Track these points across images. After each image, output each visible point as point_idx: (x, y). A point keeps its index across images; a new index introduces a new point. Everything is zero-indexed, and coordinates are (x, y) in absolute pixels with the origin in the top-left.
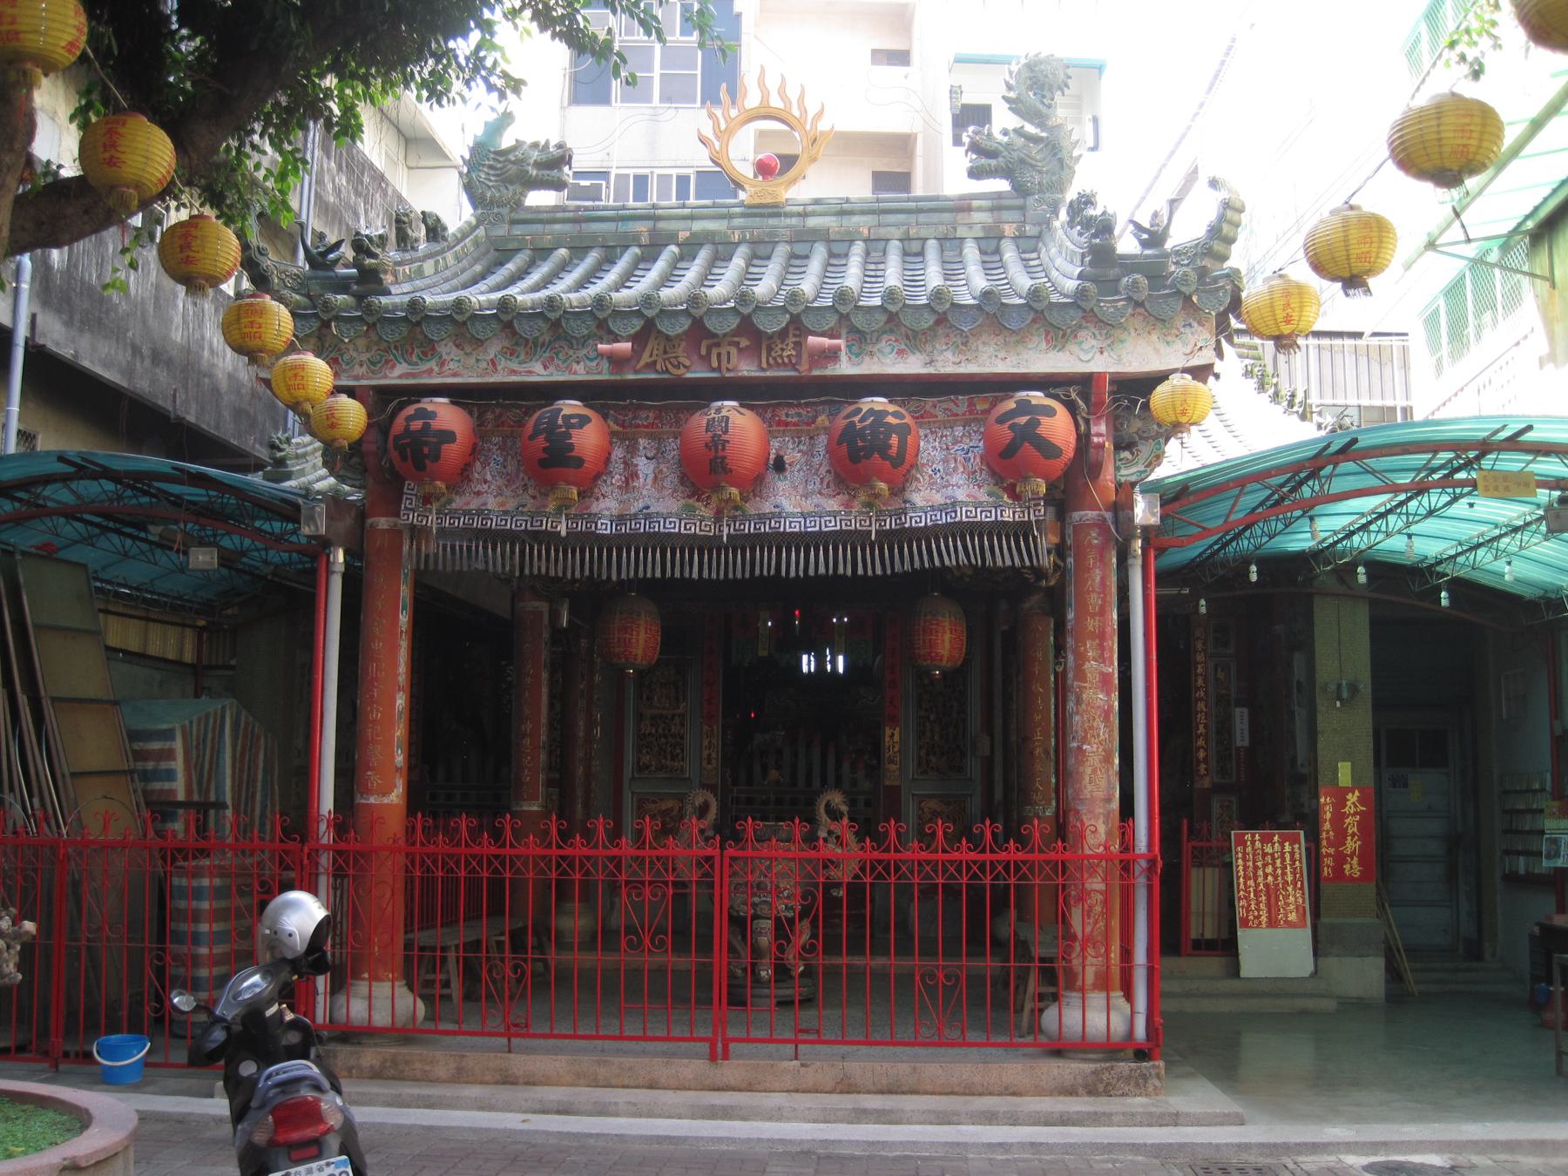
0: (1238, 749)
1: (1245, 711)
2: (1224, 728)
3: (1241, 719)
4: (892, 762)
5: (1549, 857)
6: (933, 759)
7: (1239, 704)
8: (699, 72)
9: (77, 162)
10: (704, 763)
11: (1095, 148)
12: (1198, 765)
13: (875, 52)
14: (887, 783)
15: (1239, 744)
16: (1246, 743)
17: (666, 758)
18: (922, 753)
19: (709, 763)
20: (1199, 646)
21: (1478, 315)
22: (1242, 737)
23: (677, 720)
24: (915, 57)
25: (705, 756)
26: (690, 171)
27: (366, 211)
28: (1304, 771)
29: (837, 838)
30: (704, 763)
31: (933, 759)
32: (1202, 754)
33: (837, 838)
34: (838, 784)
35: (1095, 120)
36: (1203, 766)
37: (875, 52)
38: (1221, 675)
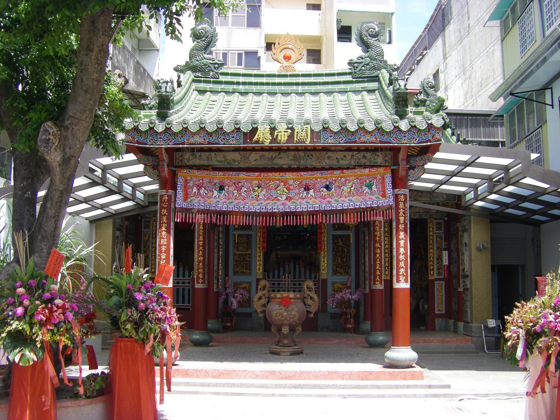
0: (444, 265)
1: (447, 252)
2: (440, 258)
3: (445, 254)
4: (324, 270)
5: (554, 293)
6: (338, 269)
7: (445, 250)
8: (246, 15)
9: (497, 299)
10: (258, 271)
11: (390, 42)
12: (430, 271)
13: (308, 5)
14: (322, 278)
15: (445, 264)
16: (447, 264)
17: (243, 269)
18: (335, 267)
19: (259, 270)
20: (431, 229)
21: (528, 115)
22: (445, 262)
23: (248, 255)
24: (323, 7)
25: (258, 268)
26: (243, 52)
27: (128, 68)
28: (468, 273)
29: (311, 297)
30: (258, 271)
31: (338, 269)
32: (432, 268)
33: (311, 297)
34: (310, 278)
35: (390, 32)
36: (432, 272)
37: (308, 5)
38: (438, 239)
